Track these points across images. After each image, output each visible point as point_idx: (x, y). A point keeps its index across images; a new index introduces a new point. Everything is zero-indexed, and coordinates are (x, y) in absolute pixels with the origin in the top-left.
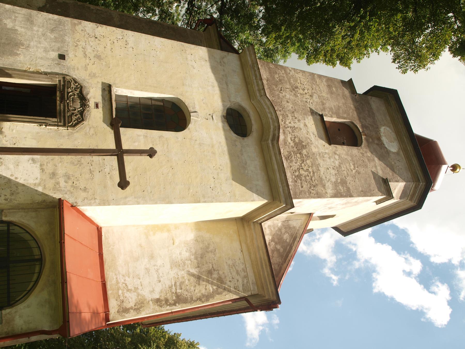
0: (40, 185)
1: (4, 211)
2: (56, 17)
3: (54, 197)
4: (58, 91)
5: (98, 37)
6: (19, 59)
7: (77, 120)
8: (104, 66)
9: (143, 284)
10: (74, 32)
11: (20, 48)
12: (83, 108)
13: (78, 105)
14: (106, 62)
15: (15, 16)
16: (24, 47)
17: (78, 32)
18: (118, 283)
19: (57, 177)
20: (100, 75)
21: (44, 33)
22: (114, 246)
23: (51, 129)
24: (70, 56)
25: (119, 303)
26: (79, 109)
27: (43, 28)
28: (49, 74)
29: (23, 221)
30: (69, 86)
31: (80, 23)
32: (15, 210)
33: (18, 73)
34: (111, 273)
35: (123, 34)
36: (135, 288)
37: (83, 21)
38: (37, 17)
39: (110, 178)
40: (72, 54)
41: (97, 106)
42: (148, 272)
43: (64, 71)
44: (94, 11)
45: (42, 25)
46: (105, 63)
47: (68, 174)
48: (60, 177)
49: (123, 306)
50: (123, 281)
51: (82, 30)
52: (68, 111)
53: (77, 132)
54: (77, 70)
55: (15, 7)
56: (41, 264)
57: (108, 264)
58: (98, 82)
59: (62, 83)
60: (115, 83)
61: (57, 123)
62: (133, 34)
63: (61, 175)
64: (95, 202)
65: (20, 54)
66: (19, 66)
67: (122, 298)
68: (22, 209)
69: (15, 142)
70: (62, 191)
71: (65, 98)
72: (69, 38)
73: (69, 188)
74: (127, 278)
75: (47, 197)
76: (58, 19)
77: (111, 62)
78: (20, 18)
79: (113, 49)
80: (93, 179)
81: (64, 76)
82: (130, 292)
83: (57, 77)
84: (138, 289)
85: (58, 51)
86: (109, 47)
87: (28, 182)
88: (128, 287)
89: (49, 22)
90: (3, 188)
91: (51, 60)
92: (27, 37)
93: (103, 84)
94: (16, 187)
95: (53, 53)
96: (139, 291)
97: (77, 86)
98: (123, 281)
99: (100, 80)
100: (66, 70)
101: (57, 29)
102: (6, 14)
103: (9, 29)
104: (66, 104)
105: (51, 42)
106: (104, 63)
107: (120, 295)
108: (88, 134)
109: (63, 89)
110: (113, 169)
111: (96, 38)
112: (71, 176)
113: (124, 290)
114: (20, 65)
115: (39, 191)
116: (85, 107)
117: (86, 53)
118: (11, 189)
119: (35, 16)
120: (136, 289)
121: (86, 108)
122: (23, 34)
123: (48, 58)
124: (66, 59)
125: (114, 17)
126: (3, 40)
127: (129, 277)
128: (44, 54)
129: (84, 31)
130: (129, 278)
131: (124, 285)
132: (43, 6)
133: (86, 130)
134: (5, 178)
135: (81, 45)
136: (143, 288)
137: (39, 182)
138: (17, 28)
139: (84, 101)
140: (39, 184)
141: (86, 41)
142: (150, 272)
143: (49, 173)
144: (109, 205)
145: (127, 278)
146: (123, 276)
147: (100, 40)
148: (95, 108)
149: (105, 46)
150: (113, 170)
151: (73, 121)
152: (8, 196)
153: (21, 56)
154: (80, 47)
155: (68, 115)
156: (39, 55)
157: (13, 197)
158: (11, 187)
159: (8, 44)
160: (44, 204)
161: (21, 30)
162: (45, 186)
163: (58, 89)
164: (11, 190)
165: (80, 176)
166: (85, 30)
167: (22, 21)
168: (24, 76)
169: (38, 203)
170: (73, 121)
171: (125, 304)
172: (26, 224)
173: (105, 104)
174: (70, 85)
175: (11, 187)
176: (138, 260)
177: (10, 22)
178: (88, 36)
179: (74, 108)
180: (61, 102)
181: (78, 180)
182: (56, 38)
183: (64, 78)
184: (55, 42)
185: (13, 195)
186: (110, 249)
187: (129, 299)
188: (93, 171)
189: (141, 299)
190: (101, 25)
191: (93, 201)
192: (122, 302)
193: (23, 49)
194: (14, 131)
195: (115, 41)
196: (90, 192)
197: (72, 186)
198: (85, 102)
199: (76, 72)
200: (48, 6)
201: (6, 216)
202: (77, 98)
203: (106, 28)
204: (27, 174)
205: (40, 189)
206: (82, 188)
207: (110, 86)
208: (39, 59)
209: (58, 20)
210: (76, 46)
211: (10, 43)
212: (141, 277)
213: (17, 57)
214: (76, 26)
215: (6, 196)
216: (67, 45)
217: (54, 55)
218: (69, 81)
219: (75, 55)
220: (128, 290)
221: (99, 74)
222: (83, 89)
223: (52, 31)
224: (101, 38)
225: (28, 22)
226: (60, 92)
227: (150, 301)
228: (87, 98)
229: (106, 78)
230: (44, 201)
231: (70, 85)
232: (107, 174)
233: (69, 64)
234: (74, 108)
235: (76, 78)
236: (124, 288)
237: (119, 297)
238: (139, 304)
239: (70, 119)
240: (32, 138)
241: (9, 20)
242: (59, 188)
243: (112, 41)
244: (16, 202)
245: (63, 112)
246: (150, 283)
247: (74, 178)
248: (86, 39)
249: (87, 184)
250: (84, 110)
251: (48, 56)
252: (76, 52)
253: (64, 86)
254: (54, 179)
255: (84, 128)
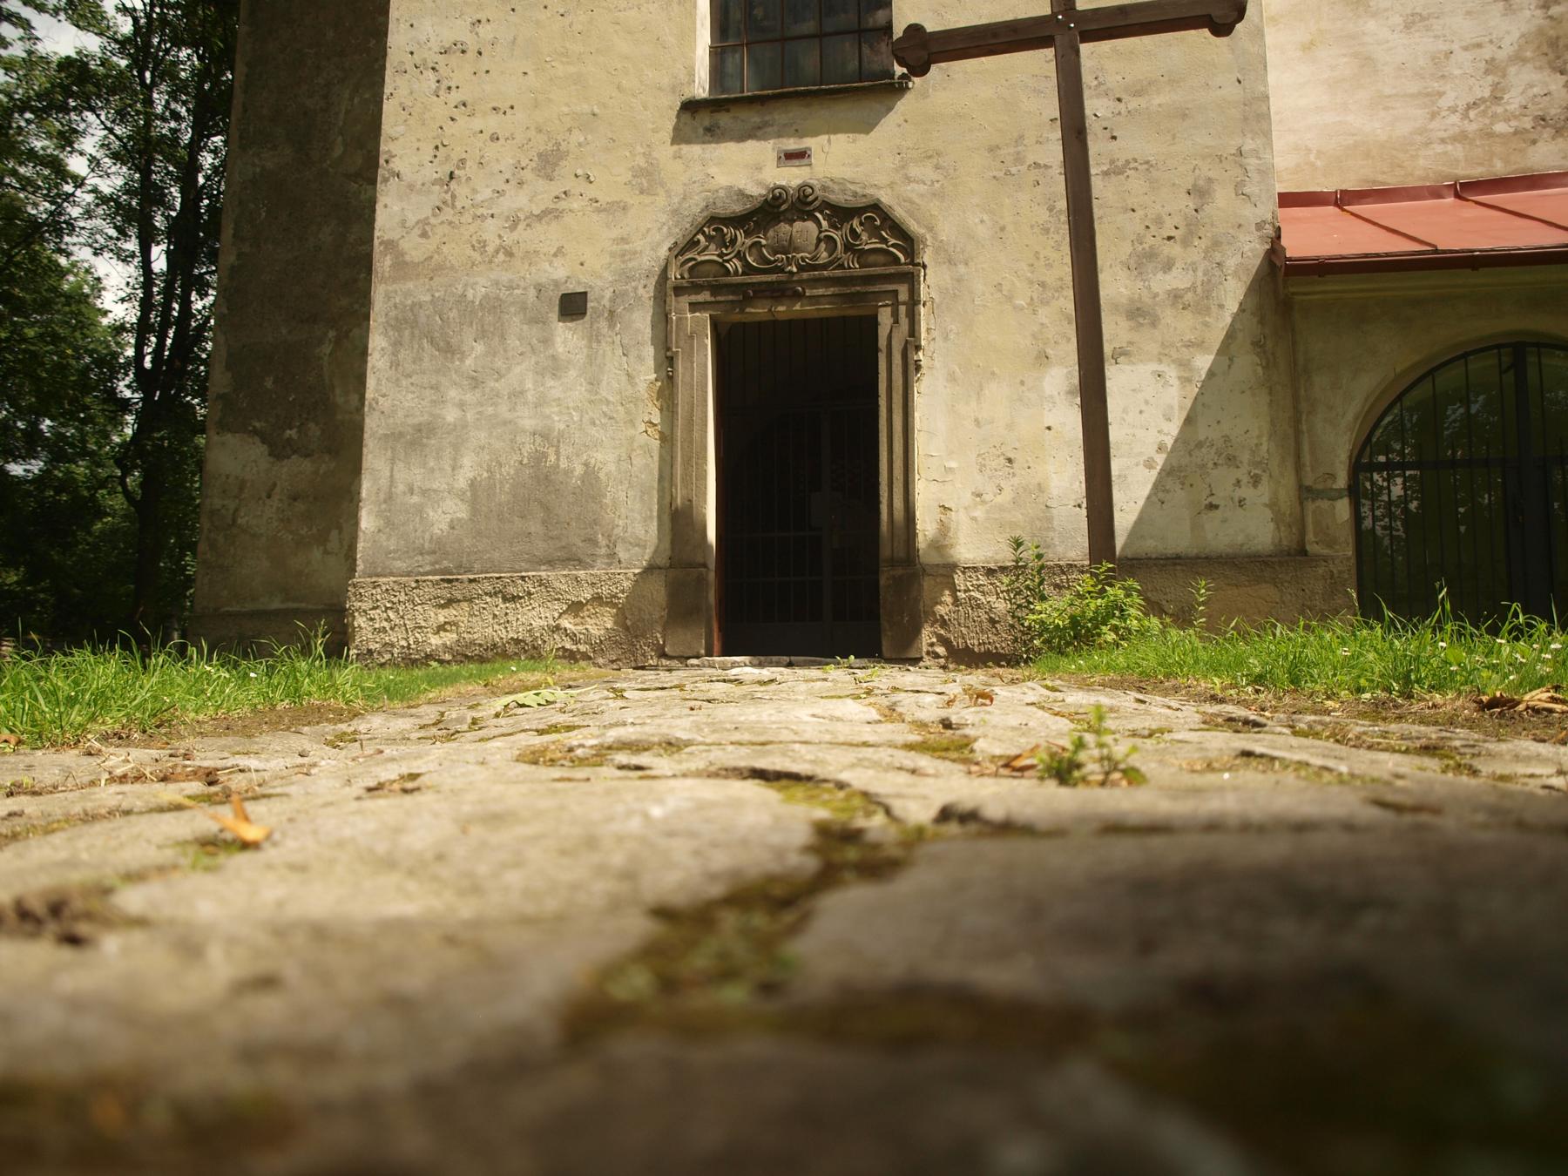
0: (1189, 360)
1: (1308, 482)
2: (377, 342)
3: (1235, 311)
4: (742, 311)
5: (447, 169)
6: (612, 467)
7: (875, 232)
8: (590, 137)
9: (1474, 41)
10: (440, 268)
11: (558, 466)
12: (814, 210)
13: (805, 231)
14: (570, 130)
15: (405, 493)
16: (551, 451)
17: (438, 250)
18: (1461, 137)
19: (1147, 299)
20: (639, 149)
21: (466, 383)
22: (1309, 150)
23: (928, 330)
24: (562, 274)
25: (1547, 133)
26: (825, 224)
27: (442, 389)
28: (669, 349)
29: (1350, 416)
30: (715, 268)
31: (390, 245)
32: (1306, 447)
33: (683, 464)
34: (1421, 162)
35: (409, 67)
36: (1487, 72)
37: (377, 233)
38: (394, 412)
39: (1138, 93)
40: (550, 269)
41: (796, 156)
42: (1423, 19)
43: (641, 291)
44: (246, 249)
45: (428, 392)
46: (576, 132)
47: (1132, 261)
48: (1149, 288)
49: (1563, 117)
50: (1455, 119)
51: (424, 235)
52: (841, 266)
53: (930, 229)
54: (627, 243)
55: (364, 494)
56: (1538, 345)
57: (1384, 173)
58: (677, 156)
59: (705, 296)
60: (673, 89)
61: (902, 309)
62: (404, 26)
63: (1140, 284)
64: (1256, 153)
65: (586, 464)
66: (647, 465)
67: (1527, 123)
68: (1296, 421)
69: (1002, 458)
70: (1209, 281)
71: (781, 282)
72: (476, 283)
73: (1195, 254)
74: (1444, 103)
75: (1240, 335)
76: (385, 334)
77: (566, 109)
78: (410, 474)
79: (495, 105)
80: (1147, 162)
81: (664, 290)
82: (1504, 91)
83: (679, 319)
84: (1493, 59)
85: (544, 323)
86: (493, 123)
87: (1176, 407)
88: (1483, 100)
89: (409, 367)
90: (1208, 492)
91: (594, 345)
92: (498, 445)
93: (679, 137)
94: (1202, 447)
95: (558, 340)
96: (1501, 55)
97: (709, 238)
98: (1455, 119)
99: (665, 151)
100: (633, 284)
101: (437, 334)
102: (403, 524)
103: (475, 511)
104: (805, 275)
105: (505, 351)
106: (577, 137)
107: (1512, 130)
108: (937, 185)
109: (733, 293)
110: (1096, 83)
111: (452, 176)
112: (1140, 248)
113: (1495, 116)
114: (638, 461)
115: (1212, 364)
116: (810, 199)
117: (536, 212)
118: (1210, 465)
119: (391, 420)
120: (1492, 66)
121: (816, 199)
122: (488, 457)
123: (591, 359)
124: (581, 290)
125: (258, 170)
126: (533, 529)
127: (1441, 94)
128: (573, 373)
129: (427, 228)
130: (1444, 93)
131: (1472, 114)
132: (263, 443)
133: (922, 196)
134: (1158, 486)
135: (500, 236)
136: (1491, 42)
137: (1173, 366)
138: (462, 482)
139: (784, 207)
140: (1184, 364)
141: (476, 217)
142: (1425, 13)
143: (1131, 329)
144: (1266, 98)
145: (1444, 103)
146: (1433, 115)
147: (463, 161)
148: (810, 165)
149: (486, 136)
150: (1100, 84)
151: (884, 246)
152: (1242, 474)
153: (593, 461)
154: (509, 238)
155: (857, 266)
156: (580, 392)
157: (1245, 457)
158: (1203, 466)
159: (547, 509)
160: (1269, 344)
161: (469, 467)
162: (1189, 345)
163: (736, 317)
164: (1215, 464)
165: (1140, 213)
166: (417, 223)
167: (424, 465)
168: (691, 442)
169: (1266, 368)
170: (884, 246)
171: (1553, 112)
172: (1363, 407)
173: (785, 125)
174: (707, 267)
175: (1203, 466)
176: (1368, 58)
177: (440, 511)
178: (446, 209)
179: (823, 245)
180: (798, 296)
181: (1159, 221)
182: (482, 335)
183: (679, 291)
184: (503, 338)
185: (1234, 457)
186: (1319, 163)
187: (1535, 96)
188: (1112, 162)
189: (1539, 47)
190: (382, 161)
191: (1252, 162)
192: (1543, 120)
193: (558, 453)
194: (953, 464)
195: (455, 97)
196: (1211, 174)
197: (1186, 243)
198: (784, 202)
199: (638, 245)
200: (257, 425)
201: (1333, 476)
202: (771, 233)
203: (393, 139)
204: (1141, 412)
205: (1203, 362)
206: (1187, 204)
207: (691, 107)
208: (597, 393)
209: (391, 333)
210: (510, 254)
211: (541, 503)
212: (1445, 48)
213: (602, 475)
214: (407, 258)
215: (1239, 482)
216: (510, 288)
217: (567, 337)
218: (691, 269)
219: (555, 255)
220: (1496, 100)
221: (635, 155)
222: (721, 212)
223: (449, 350)
224: (448, 158)
225: (425, 445)
226: (747, 300)
227: (1550, 13)
228: (760, 195)
229: (650, 126)
230: (1256, 344)
231: (707, 267)
232: (1122, 107)
233: (606, 274)
234: (823, 245)
235: (668, 244)
236: (1484, 113)
237: (1522, 133)
238: (1558, 58)
239: (872, 258)
240: (979, 399)
241: (431, 514)
242: (1199, 290)
243: (455, 113)
244: (1265, 447)
245: (845, 286)
246: (1468, 13)
247: (1149, 236)
248: (467, 218)
249: (1174, 184)
250: (826, 205)
251: (581, 358)
252: (536, 252)
253: (716, 289)
254: (1159, 312)
255: (912, 202)
